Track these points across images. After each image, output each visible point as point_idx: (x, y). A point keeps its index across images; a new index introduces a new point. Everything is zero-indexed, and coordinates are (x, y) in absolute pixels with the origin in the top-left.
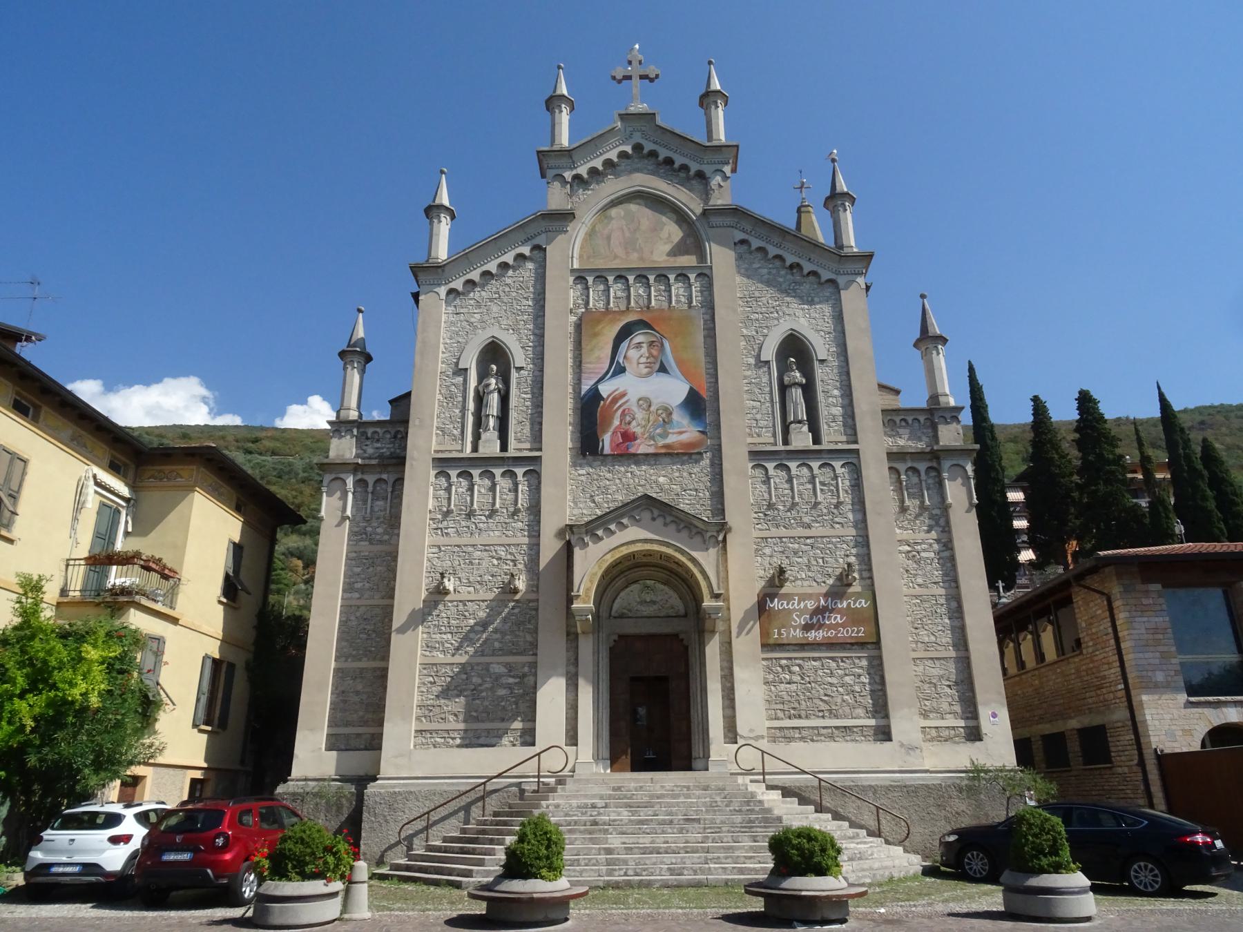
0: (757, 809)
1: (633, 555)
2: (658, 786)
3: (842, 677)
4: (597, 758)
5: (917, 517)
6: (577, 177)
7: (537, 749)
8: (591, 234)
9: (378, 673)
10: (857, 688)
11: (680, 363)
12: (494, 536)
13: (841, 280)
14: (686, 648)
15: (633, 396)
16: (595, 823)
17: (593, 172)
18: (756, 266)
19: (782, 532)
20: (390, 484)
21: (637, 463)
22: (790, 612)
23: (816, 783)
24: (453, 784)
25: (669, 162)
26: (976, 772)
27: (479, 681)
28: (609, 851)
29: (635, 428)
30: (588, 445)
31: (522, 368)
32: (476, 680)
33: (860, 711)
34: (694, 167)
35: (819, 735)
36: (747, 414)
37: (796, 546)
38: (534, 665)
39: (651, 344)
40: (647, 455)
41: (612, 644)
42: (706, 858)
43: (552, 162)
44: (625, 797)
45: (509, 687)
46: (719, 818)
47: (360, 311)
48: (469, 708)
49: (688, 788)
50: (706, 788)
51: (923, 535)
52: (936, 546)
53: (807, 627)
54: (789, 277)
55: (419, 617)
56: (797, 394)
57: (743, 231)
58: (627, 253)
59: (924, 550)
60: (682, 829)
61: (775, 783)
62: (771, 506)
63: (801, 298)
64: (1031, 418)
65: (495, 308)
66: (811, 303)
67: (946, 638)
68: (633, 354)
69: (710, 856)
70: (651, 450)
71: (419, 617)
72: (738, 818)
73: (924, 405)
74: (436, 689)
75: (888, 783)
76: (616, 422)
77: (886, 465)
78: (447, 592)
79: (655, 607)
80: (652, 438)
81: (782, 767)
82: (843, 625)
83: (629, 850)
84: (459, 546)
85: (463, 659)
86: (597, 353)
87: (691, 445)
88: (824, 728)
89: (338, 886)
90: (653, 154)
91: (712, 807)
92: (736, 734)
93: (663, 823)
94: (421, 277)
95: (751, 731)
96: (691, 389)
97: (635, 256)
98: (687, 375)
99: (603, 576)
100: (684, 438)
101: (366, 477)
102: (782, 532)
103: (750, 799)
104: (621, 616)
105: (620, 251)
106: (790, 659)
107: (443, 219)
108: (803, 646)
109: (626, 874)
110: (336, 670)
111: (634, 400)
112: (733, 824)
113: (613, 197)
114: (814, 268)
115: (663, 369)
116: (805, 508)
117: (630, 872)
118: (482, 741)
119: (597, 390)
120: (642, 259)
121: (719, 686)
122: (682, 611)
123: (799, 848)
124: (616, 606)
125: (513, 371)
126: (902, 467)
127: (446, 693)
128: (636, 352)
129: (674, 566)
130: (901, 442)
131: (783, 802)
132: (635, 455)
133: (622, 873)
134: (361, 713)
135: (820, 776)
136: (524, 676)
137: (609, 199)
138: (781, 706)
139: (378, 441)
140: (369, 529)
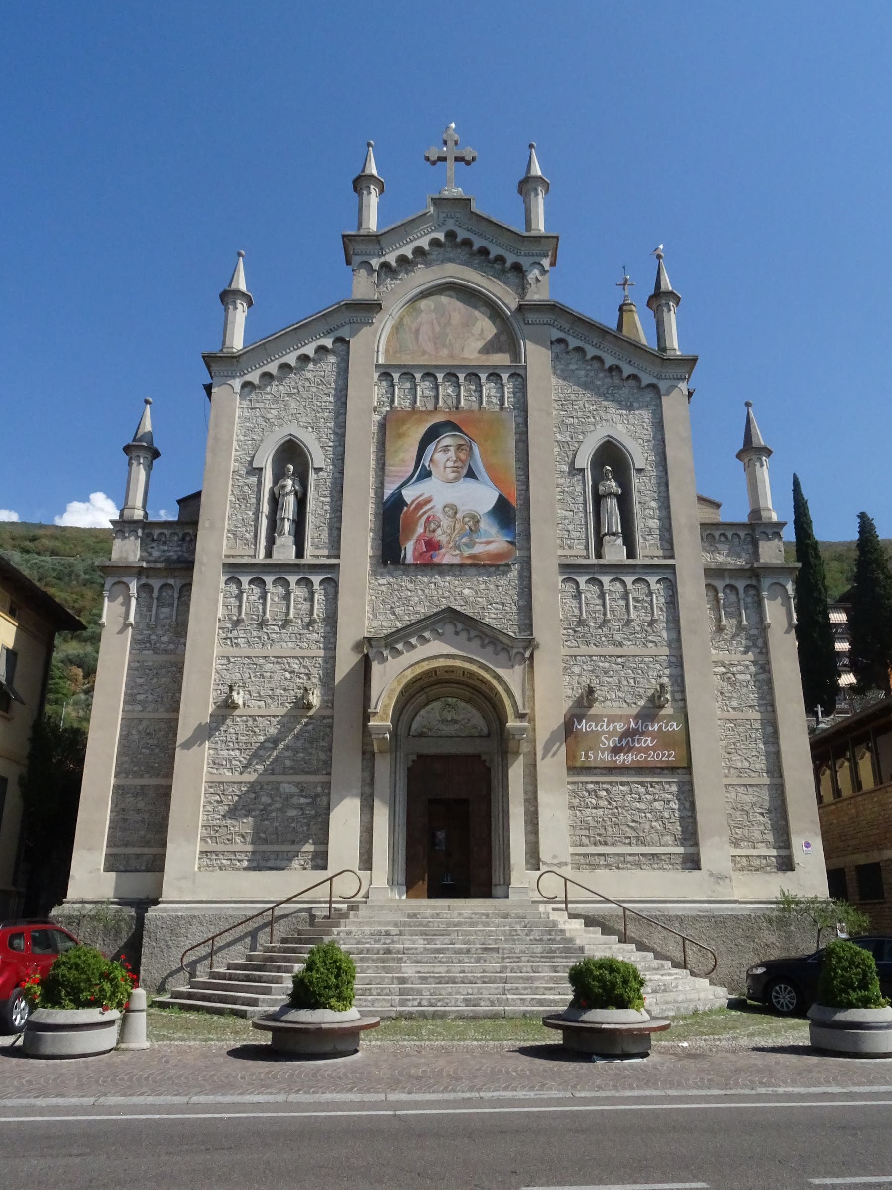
4: (392, 883)
5: (733, 638)
6: (385, 266)
7: (329, 873)
8: (398, 327)
10: (666, 815)
11: (489, 468)
13: (663, 385)
14: (489, 770)
15: (438, 503)
16: (388, 951)
19: (592, 649)
20: (177, 590)
21: (441, 574)
22: (598, 734)
23: (620, 912)
25: (484, 252)
27: (269, 801)
28: (403, 981)
29: (439, 536)
30: (389, 554)
31: (320, 470)
32: (265, 799)
33: (669, 839)
34: (510, 259)
36: (559, 523)
38: (327, 785)
39: (459, 447)
40: (452, 565)
41: (410, 764)
43: (360, 248)
44: (421, 925)
45: (301, 808)
46: (518, 947)
47: (147, 402)
48: (257, 829)
49: (487, 916)
50: (506, 916)
51: (739, 656)
52: (753, 668)
53: (616, 751)
54: (608, 380)
55: (205, 732)
56: (612, 505)
57: (561, 329)
58: (436, 349)
59: (740, 672)
60: (480, 958)
62: (581, 622)
63: (620, 403)
65: (293, 405)
66: (630, 408)
67: (761, 764)
68: (440, 457)
69: (508, 986)
70: (457, 560)
71: (205, 732)
72: (538, 948)
73: (744, 519)
74: (223, 809)
75: (695, 913)
76: (420, 530)
78: (235, 707)
80: (457, 547)
82: (654, 749)
83: (424, 980)
85: (251, 777)
86: (401, 456)
87: (500, 555)
89: (114, 1014)
90: (467, 243)
91: (512, 936)
92: (538, 860)
93: (459, 952)
94: (214, 368)
95: (554, 857)
100: (492, 548)
102: (592, 649)
104: (421, 735)
105: (429, 347)
106: (597, 783)
107: (239, 306)
108: (611, 770)
109: (419, 1005)
110: (117, 787)
115: (471, 474)
116: (617, 625)
117: (425, 1003)
120: (452, 356)
121: (521, 810)
122: (485, 731)
123: (600, 979)
124: (415, 726)
126: (720, 584)
127: (233, 813)
128: (442, 456)
130: (720, 558)
132: (439, 565)
133: (416, 1003)
135: (626, 905)
138: (586, 832)
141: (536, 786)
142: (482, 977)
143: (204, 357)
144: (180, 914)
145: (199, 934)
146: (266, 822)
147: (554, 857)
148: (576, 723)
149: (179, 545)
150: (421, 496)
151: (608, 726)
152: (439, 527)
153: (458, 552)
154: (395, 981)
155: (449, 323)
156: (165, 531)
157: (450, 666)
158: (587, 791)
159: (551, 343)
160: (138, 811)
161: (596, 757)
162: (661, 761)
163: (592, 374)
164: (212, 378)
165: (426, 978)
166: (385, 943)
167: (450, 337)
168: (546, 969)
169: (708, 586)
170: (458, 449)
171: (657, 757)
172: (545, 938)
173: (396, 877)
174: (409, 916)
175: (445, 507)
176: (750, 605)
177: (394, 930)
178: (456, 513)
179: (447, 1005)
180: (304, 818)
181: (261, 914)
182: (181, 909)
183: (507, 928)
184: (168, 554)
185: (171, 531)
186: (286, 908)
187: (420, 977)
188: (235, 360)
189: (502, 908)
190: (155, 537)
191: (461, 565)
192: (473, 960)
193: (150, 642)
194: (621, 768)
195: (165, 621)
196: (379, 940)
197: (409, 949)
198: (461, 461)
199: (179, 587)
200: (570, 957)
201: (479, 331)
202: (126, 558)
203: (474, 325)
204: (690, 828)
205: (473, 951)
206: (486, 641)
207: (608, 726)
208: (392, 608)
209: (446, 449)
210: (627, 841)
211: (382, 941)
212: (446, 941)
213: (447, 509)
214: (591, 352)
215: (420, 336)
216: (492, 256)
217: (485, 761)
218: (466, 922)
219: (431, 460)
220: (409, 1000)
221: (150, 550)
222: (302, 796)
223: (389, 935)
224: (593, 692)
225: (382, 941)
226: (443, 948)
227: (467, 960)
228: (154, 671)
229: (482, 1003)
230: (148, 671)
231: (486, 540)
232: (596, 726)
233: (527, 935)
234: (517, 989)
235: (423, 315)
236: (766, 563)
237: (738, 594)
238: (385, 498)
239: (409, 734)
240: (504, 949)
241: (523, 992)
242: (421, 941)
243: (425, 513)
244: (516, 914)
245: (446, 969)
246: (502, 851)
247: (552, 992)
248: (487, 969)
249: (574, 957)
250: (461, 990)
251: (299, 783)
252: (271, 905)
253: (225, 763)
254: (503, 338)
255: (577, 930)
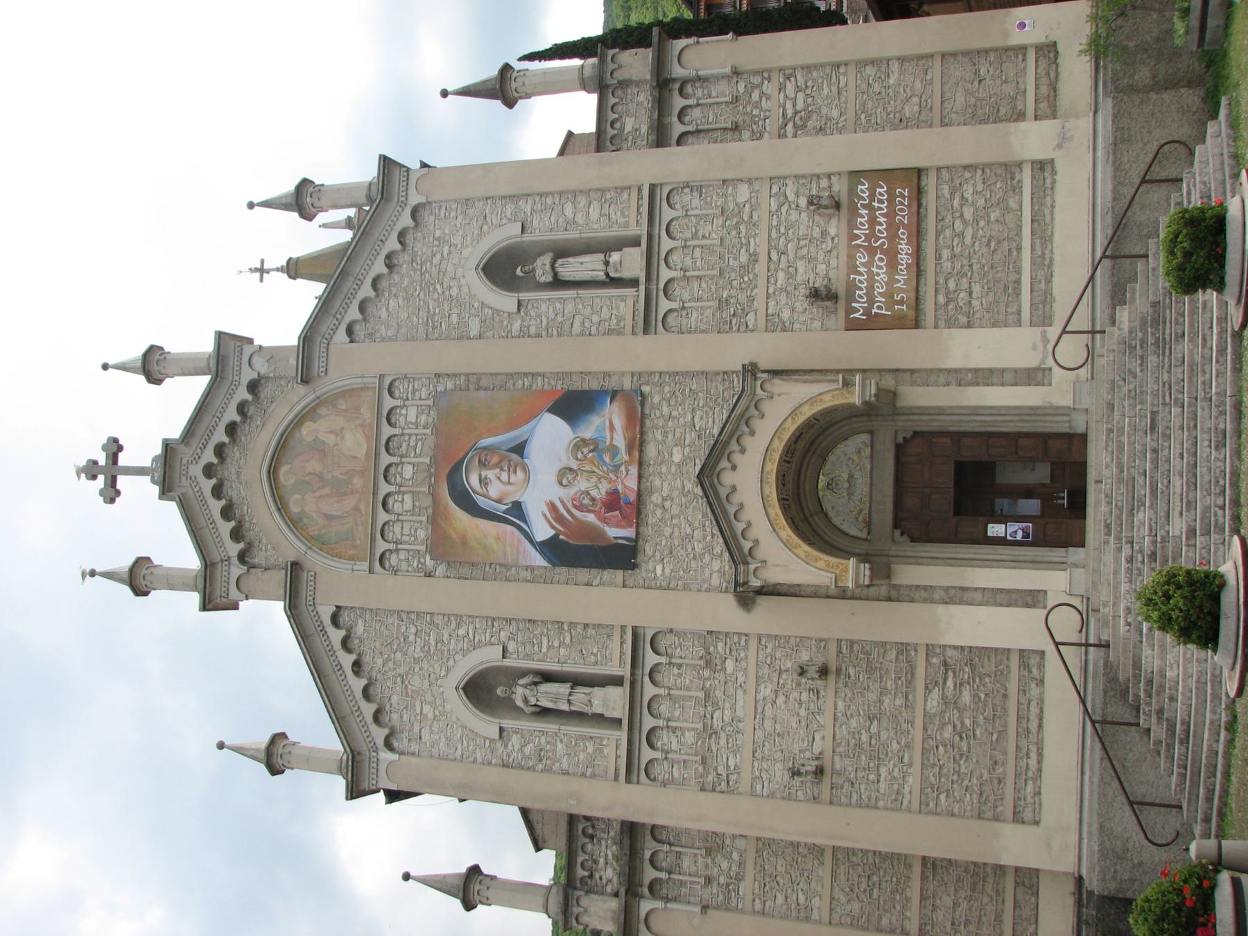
0: (1140, 335)
1: (783, 501)
2: (1106, 472)
3: (964, 222)
6: (242, 557)
7: (1050, 648)
9: (929, 873)
11: (513, 425)
12: (744, 705)
14: (916, 433)
15: (556, 493)
16: (1153, 556)
17: (236, 535)
18: (384, 314)
19: (760, 293)
20: (658, 846)
23: (1106, 262)
24: (1092, 768)
25: (232, 429)
26: (1099, 49)
27: (950, 728)
28: (1192, 533)
29: (600, 492)
30: (622, 557)
31: (504, 650)
34: (243, 394)
35: (1043, 256)
36: (587, 338)
37: (781, 275)
39: (483, 464)
40: (640, 477)
41: (906, 538)
42: (1204, 399)
43: (218, 591)
44: (1119, 517)
45: (959, 686)
46: (1151, 386)
49: (1110, 431)
50: (1111, 407)
56: (572, 268)
58: (352, 492)
59: (794, 105)
60: (1164, 435)
61: (1106, 316)
64: (594, 130)
68: (494, 490)
69: (1201, 395)
70: (634, 470)
72: (1152, 360)
73: (594, 98)
75: (1110, 169)
76: (591, 518)
77: (674, 149)
79: (857, 475)
80: (616, 468)
81: (1084, 308)
83: (1191, 505)
84: (754, 752)
86: (491, 541)
88: (1033, 249)
90: (220, 450)
91: (1137, 396)
92: (1037, 369)
93: (1155, 461)
94: (365, 785)
95: (1035, 348)
96: (550, 411)
97: (357, 482)
98: (530, 415)
99: (811, 544)
100: (619, 423)
101: (647, 881)
102: (760, 293)
103: (1128, 346)
104: (869, 524)
105: (349, 503)
106: (936, 291)
109: (1223, 508)
111: (561, 492)
112: (1160, 367)
113: (273, 508)
114: (394, 235)
115: (520, 449)
117: (1220, 501)
118: (1033, 726)
119: (543, 543)
120: (362, 473)
121: (972, 390)
122: (865, 437)
123: (1187, 255)
124: (853, 531)
125: (508, 662)
126: (678, 129)
128: (493, 487)
129: (802, 444)
131: (1133, 300)
132: (639, 494)
133: (1220, 512)
134: (985, 900)
135: (1099, 254)
136: (945, 664)
137: (276, 513)
139: (596, 862)
140: (722, 880)
141: (940, 370)
142: (1188, 430)
143: (352, 798)
144: (1096, 848)
145: (1124, 820)
146: (978, 732)
147: (1035, 348)
148: (856, 315)
149: (599, 841)
150: (545, 516)
151: (860, 274)
152: (588, 493)
153: (623, 468)
154: (1191, 542)
155: (320, 477)
156: (580, 860)
157: (777, 479)
158: (947, 304)
159: (352, 342)
160: (956, 905)
161: (902, 290)
162: (909, 206)
163: (394, 290)
164: (377, 791)
165: (1188, 503)
166: (1143, 562)
167: (337, 473)
168: (1179, 347)
169: (679, 143)
170: (484, 465)
171: (900, 210)
172: (1139, 352)
173: (1057, 559)
174: (1108, 533)
175: (561, 483)
176: (706, 92)
177: (1126, 551)
178: (571, 469)
179: (1224, 471)
180: (974, 681)
181: (1100, 739)
182: (1091, 846)
183: (1126, 403)
184: (610, 857)
185: (580, 852)
186: (1093, 700)
187: (1188, 510)
188: (357, 758)
189: (1101, 413)
190: (586, 874)
191: (641, 464)
192: (1166, 444)
193: (728, 885)
194: (918, 258)
195: (699, 864)
196: (1138, 569)
197: (1150, 529)
198: (501, 461)
199: (655, 843)
200: (1164, 317)
201: (332, 436)
202: (614, 912)
203: (323, 442)
204: (999, 172)
205: (1154, 445)
206: (747, 430)
207: (860, 274)
208: (694, 558)
209: (484, 482)
210: (1015, 253)
211: (1139, 565)
212: (1141, 481)
213: (564, 482)
214: (366, 291)
215: (334, 513)
216: (238, 418)
217: (905, 439)
218: (1118, 457)
219: (499, 501)
220: (1216, 522)
221: (604, 881)
222: (945, 683)
223: (1132, 557)
224: (816, 290)
225: (1139, 565)
226: (1151, 483)
227: (1166, 452)
228: (767, 879)
229: (1222, 426)
230: (767, 888)
231: (607, 431)
232: (861, 289)
233: (1135, 377)
234: (1204, 383)
235: (307, 509)
236: (652, 72)
237: (690, 106)
238: (546, 564)
239: (866, 540)
240: (1153, 405)
241: (1208, 376)
242: (1141, 515)
243: (568, 511)
244: (1108, 393)
245: (1177, 478)
246: (1027, 418)
247: (1208, 338)
248: (1178, 424)
249: (1164, 312)
250: (1205, 455)
251: (926, 688)
252: (1089, 724)
253: (896, 787)
254: (342, 405)
255: (1130, 313)
